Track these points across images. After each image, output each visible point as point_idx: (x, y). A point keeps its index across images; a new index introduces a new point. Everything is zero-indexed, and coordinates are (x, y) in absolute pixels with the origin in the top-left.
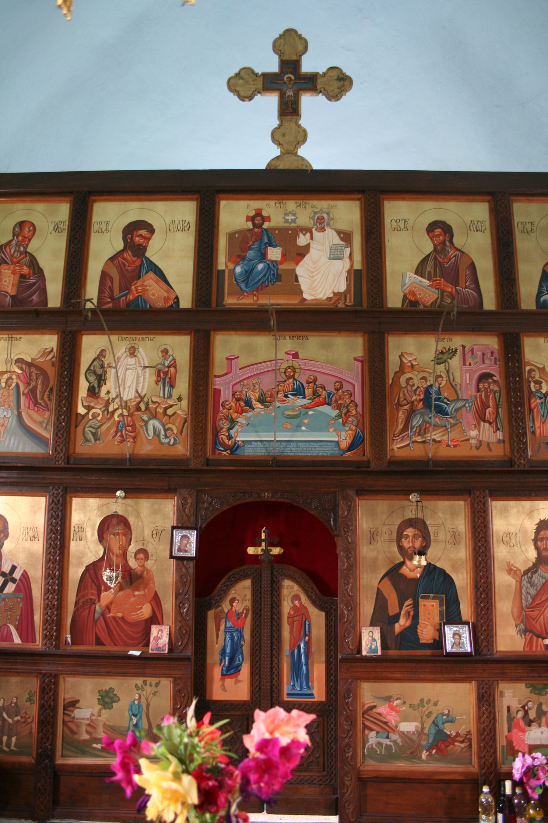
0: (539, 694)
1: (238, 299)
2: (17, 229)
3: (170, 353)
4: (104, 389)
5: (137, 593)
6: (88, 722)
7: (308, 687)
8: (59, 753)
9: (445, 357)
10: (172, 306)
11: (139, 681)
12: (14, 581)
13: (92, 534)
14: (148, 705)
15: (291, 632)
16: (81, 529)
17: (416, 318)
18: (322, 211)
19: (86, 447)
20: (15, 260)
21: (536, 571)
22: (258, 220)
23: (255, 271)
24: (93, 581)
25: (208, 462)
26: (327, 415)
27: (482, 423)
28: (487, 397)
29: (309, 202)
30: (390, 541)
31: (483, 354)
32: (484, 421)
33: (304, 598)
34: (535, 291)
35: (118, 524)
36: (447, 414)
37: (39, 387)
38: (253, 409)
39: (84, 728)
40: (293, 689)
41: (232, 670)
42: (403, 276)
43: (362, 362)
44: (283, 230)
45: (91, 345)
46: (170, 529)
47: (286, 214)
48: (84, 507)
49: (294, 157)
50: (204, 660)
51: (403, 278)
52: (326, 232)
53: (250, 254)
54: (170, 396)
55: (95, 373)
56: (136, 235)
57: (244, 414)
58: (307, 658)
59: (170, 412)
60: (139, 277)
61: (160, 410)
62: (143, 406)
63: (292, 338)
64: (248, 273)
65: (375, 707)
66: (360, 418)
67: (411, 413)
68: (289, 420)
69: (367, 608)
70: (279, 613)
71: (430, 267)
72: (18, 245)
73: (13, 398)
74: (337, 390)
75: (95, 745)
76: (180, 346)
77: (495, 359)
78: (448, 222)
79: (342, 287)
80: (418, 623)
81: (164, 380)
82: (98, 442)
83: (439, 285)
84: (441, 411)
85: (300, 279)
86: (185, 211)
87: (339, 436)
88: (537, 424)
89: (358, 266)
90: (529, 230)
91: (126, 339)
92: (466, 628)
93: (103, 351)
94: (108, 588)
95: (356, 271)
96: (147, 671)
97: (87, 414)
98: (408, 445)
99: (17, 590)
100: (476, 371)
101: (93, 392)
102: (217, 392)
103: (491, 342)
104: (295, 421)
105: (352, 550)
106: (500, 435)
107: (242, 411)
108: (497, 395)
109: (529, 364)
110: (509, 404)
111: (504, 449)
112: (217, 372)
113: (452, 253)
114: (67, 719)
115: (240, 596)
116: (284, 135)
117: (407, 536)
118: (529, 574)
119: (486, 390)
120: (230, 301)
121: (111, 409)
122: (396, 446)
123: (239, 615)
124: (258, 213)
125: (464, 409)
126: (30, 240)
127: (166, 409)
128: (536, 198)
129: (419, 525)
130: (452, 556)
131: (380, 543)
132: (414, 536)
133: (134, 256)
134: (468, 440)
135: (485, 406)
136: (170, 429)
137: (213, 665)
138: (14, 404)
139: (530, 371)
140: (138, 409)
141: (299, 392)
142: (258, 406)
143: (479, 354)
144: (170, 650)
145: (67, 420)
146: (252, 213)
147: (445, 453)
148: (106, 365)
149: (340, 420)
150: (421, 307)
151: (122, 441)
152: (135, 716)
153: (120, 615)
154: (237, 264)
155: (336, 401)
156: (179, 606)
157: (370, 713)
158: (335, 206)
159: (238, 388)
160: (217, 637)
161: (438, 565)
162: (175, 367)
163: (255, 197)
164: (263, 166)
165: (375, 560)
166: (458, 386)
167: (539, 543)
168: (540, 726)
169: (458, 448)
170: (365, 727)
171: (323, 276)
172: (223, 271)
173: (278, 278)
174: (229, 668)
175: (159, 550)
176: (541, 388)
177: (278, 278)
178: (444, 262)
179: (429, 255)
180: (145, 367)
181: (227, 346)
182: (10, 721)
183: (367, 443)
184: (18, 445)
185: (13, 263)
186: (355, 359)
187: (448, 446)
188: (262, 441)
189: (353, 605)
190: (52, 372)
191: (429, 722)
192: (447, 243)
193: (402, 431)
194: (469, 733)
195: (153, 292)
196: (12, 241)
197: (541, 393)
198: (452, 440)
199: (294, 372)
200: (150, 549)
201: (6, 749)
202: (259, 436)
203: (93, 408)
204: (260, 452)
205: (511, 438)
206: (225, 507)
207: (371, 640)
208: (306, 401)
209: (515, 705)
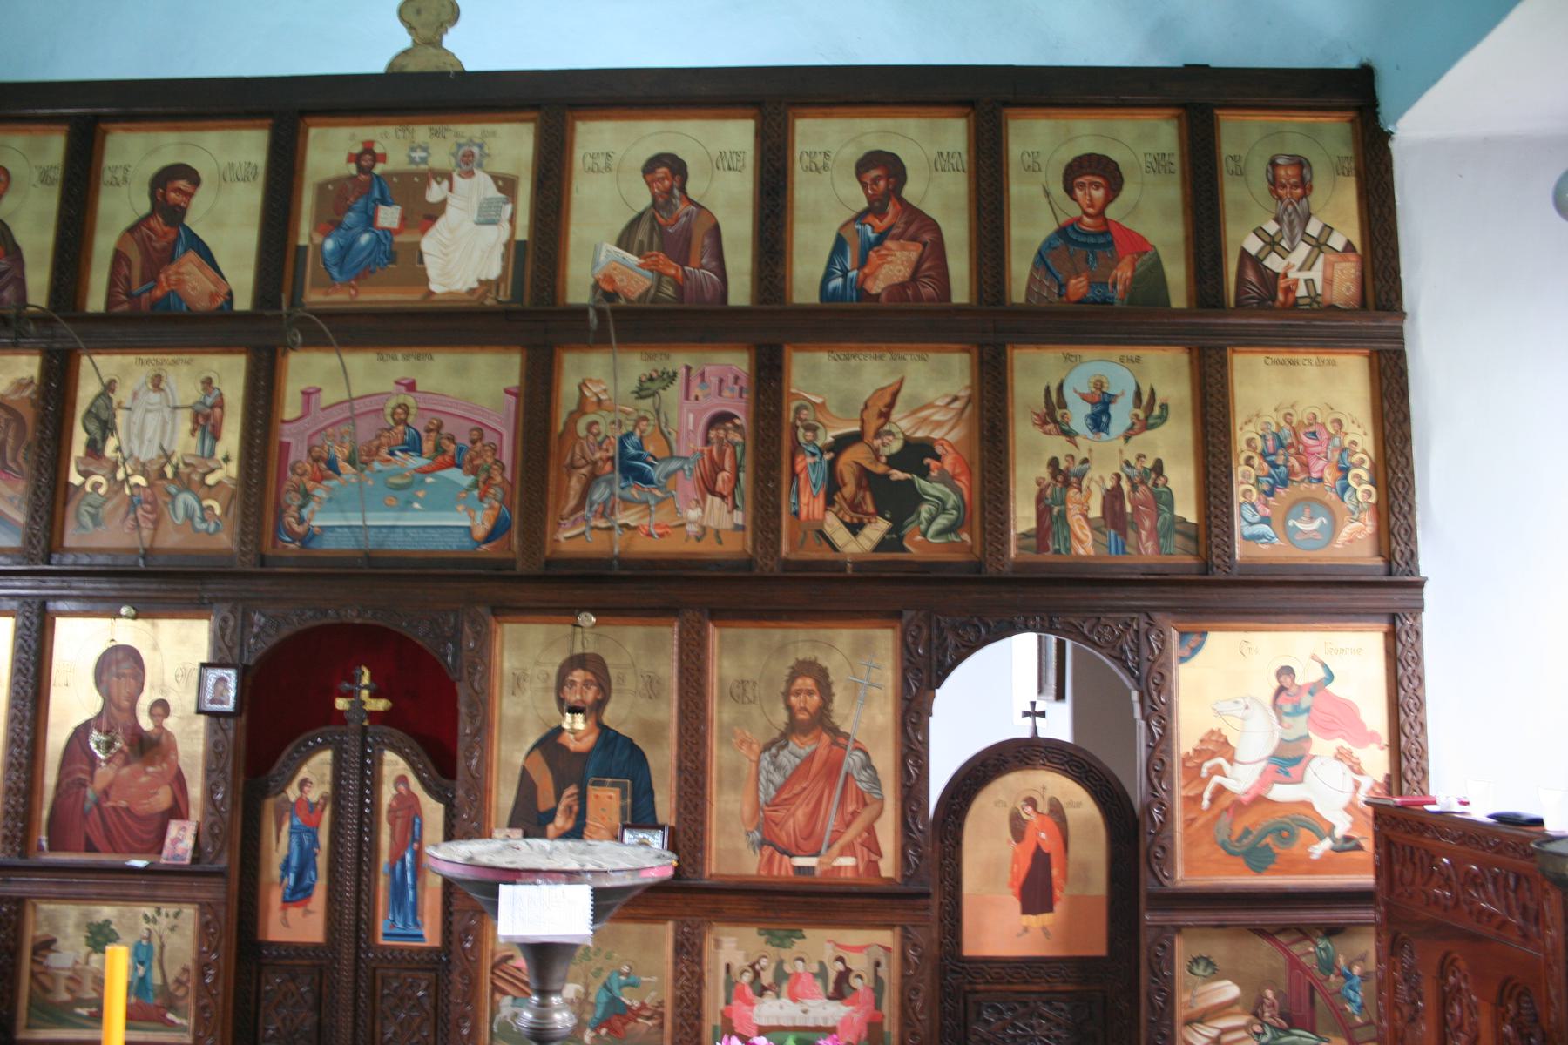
0: (781, 946)
3: (215, 384)
5: (150, 769)
6: (68, 973)
7: (416, 924)
10: (221, 308)
15: (392, 836)
18: (471, 142)
21: (786, 745)
23: (356, 246)
26: (454, 484)
27: (709, 497)
28: (722, 454)
29: (452, 127)
31: (721, 381)
32: (714, 493)
33: (413, 782)
34: (820, 271)
36: (648, 481)
37: (10, 440)
38: (339, 474)
39: (62, 983)
40: (393, 926)
41: (299, 894)
42: (597, 249)
44: (405, 176)
46: (197, 667)
47: (413, 149)
51: (597, 254)
52: (475, 179)
53: (350, 218)
54: (212, 454)
55: (97, 417)
56: (172, 185)
57: (325, 483)
58: (415, 877)
61: (196, 477)
62: (169, 471)
63: (406, 358)
64: (344, 251)
65: (511, 957)
66: (507, 487)
68: (397, 493)
70: (376, 805)
71: (642, 235)
74: (474, 442)
75: (79, 1010)
76: (229, 373)
77: (741, 389)
78: (681, 156)
80: (585, 825)
81: (204, 428)
83: (656, 263)
85: (427, 259)
86: (249, 147)
87: (473, 519)
88: (804, 499)
89: (522, 235)
90: (820, 165)
91: (148, 362)
96: (160, 893)
98: (583, 533)
100: (706, 409)
101: (94, 449)
102: (285, 448)
103: (738, 362)
104: (401, 495)
105: (483, 705)
106: (738, 517)
108: (739, 449)
109: (797, 396)
110: (757, 465)
111: (744, 540)
113: (682, 208)
114: (37, 968)
115: (315, 775)
116: (419, 12)
117: (573, 683)
118: (774, 750)
119: (720, 440)
122: (563, 535)
123: (312, 807)
124: (368, 148)
125: (680, 474)
128: (835, 110)
129: (594, 665)
132: (586, 684)
134: (683, 525)
135: (717, 467)
137: (271, 884)
139: (798, 410)
140: (163, 475)
141: (414, 446)
143: (715, 380)
144: (195, 860)
146: (358, 149)
147: (643, 546)
148: (115, 405)
149: (476, 493)
150: (622, 302)
152: (142, 963)
153: (123, 804)
154: (327, 235)
155: (471, 460)
156: (210, 791)
157: (504, 966)
158: (494, 134)
159: (317, 441)
161: (622, 730)
162: (222, 407)
163: (364, 119)
164: (378, 66)
165: (518, 723)
166: (674, 435)
167: (793, 699)
168: (778, 996)
169: (666, 539)
170: (495, 988)
171: (465, 252)
172: (305, 248)
173: (392, 257)
175: (182, 700)
176: (815, 437)
177: (392, 257)
178: (668, 224)
179: (641, 216)
180: (176, 408)
181: (309, 372)
183: (515, 529)
186: (507, 391)
187: (650, 535)
188: (350, 527)
190: (29, 414)
192: (676, 192)
193: (580, 506)
194: (661, 1004)
195: (193, 282)
197: (815, 446)
198: (657, 526)
199: (407, 413)
202: (346, 519)
203: (93, 473)
204: (347, 544)
205: (754, 522)
208: (421, 462)
209: (739, 961)
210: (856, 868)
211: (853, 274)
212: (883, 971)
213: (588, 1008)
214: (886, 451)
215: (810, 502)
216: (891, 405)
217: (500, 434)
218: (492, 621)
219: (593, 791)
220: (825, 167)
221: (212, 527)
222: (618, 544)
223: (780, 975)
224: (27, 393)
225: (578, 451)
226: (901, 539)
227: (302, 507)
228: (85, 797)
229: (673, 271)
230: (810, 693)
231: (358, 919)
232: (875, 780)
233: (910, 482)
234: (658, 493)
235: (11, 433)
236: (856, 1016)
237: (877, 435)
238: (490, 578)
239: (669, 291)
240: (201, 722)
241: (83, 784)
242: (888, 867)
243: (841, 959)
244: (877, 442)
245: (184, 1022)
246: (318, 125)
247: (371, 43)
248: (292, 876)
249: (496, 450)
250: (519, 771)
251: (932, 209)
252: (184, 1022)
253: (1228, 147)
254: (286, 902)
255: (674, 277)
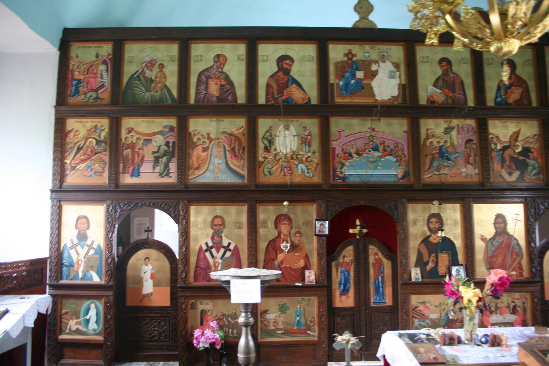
1: (342, 99)
2: (216, 59)
4: (273, 148)
5: (296, 254)
7: (384, 299)
8: (259, 337)
9: (449, 130)
10: (306, 103)
11: (299, 298)
12: (230, 250)
13: (271, 225)
14: (305, 311)
15: (374, 272)
16: (265, 222)
17: (435, 110)
18: (383, 51)
19: (265, 178)
20: (217, 76)
22: (350, 56)
24: (273, 249)
25: (332, 186)
26: (390, 161)
27: (468, 165)
28: (470, 151)
30: (424, 225)
31: (468, 129)
33: (380, 255)
35: (285, 219)
36: (450, 160)
37: (237, 147)
39: (272, 324)
41: (345, 292)
43: (407, 133)
44: (364, 62)
45: (264, 124)
47: (365, 53)
48: (414, 211)
49: (367, 21)
50: (331, 287)
51: (427, 90)
53: (347, 75)
55: (267, 139)
56: (284, 62)
58: (383, 284)
59: (309, 159)
60: (287, 87)
61: (304, 159)
62: (295, 157)
64: (347, 85)
65: (417, 307)
67: (433, 159)
69: (413, 258)
71: (440, 83)
72: (218, 68)
73: (222, 153)
74: (395, 148)
75: (278, 332)
79: (396, 93)
80: (438, 265)
82: (272, 174)
84: (448, 159)
87: (397, 172)
88: (495, 165)
92: (462, 267)
93: (271, 127)
94: (282, 251)
95: (403, 84)
97: (264, 161)
99: (232, 255)
101: (267, 149)
102: (334, 149)
103: (471, 122)
104: (374, 164)
105: (405, 230)
107: (347, 159)
108: (475, 150)
112: (333, 138)
114: (262, 319)
115: (348, 254)
117: (432, 222)
120: (338, 100)
121: (277, 158)
123: (348, 264)
124: (350, 52)
126: (224, 65)
127: (307, 158)
129: (438, 216)
130: (453, 232)
131: (419, 226)
132: (436, 222)
133: (284, 75)
135: (469, 156)
136: (309, 169)
137: (335, 289)
138: (223, 156)
139: (492, 138)
140: (292, 158)
141: (376, 149)
142: (355, 156)
143: (466, 129)
144: (316, 282)
145: (254, 165)
146: (347, 52)
147: (450, 180)
148: (273, 135)
150: (436, 104)
151: (285, 175)
152: (298, 316)
153: (288, 266)
154: (340, 80)
156: (319, 260)
159: (344, 147)
160: (337, 275)
170: (413, 317)
171: (386, 86)
173: (363, 88)
174: (343, 291)
177: (363, 88)
181: (338, 124)
182: (232, 322)
184: (227, 179)
185: (217, 78)
189: (406, 257)
191: (444, 314)
192: (449, 70)
195: (296, 95)
196: (213, 65)
200: (302, 231)
201: (231, 336)
204: (357, 180)
206: (342, 209)
207: (416, 274)
208: (379, 154)
210: (516, 275)
211: (503, 97)
212: (525, 305)
213: (441, 321)
214: (517, 151)
215: (496, 166)
216: (517, 137)
217: (403, 145)
218: (407, 203)
219: (440, 255)
220: (201, 60)
221: (311, 175)
222: (444, 179)
223: (497, 308)
224: (241, 130)
225: (428, 151)
226: (523, 177)
227: (341, 168)
228: (275, 264)
229: (450, 95)
230: (501, 223)
231: (366, 298)
232: (520, 249)
233: (524, 160)
234: (453, 164)
235: (237, 144)
236: (519, 319)
237: (515, 146)
238: (406, 190)
239: (450, 101)
240: (315, 238)
241: (274, 260)
242: (526, 274)
243: (513, 302)
244: (514, 148)
245: (314, 334)
246: (332, 44)
247: (347, 19)
248: (342, 286)
249: (402, 150)
250: (417, 250)
251: (525, 77)
252: (314, 334)
253: (127, 55)
254: (341, 295)
255: (451, 96)
